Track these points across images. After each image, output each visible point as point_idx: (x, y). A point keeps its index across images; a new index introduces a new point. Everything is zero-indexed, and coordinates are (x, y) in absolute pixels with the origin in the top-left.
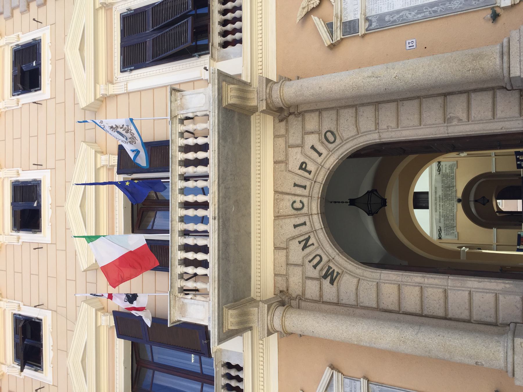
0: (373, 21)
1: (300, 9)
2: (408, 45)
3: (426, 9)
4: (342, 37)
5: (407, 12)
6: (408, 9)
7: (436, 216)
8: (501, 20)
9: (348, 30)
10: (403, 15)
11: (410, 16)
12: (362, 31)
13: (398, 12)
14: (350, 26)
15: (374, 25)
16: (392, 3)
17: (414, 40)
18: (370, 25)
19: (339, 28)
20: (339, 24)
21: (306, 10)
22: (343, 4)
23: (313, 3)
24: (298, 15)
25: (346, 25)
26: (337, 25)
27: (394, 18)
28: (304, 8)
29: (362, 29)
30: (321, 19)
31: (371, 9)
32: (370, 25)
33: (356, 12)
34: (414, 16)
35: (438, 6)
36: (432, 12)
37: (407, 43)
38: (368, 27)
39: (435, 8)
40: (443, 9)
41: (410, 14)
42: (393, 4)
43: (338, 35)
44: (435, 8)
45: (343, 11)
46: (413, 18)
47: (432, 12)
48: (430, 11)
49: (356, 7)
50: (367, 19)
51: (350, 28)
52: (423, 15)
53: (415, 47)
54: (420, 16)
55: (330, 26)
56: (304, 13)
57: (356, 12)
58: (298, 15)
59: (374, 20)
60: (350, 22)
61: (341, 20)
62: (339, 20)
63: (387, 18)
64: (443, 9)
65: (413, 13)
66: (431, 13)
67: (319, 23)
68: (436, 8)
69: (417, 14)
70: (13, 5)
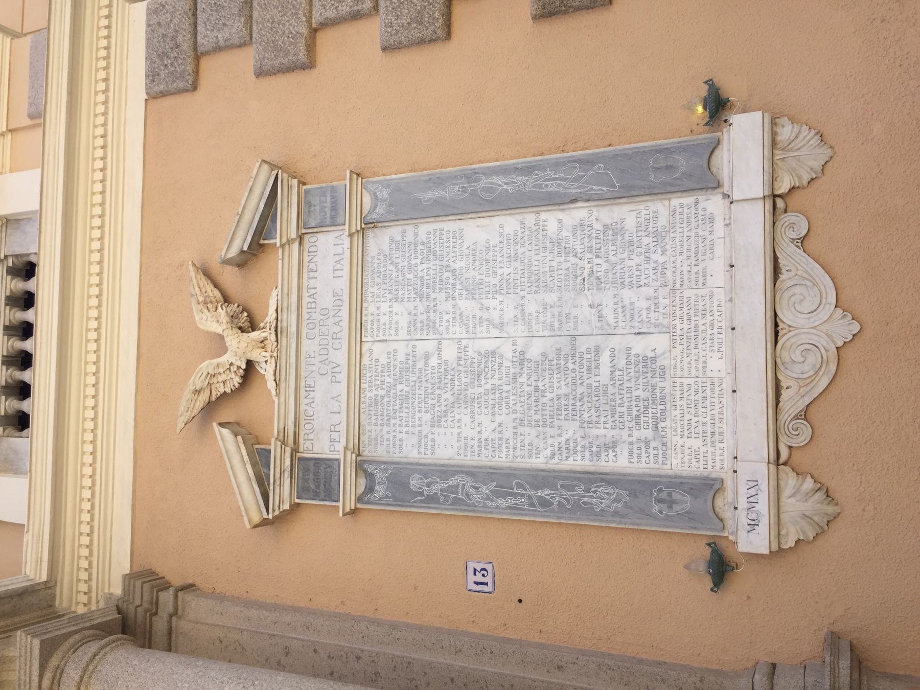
0: (378, 480)
1: (187, 395)
2: (472, 578)
3: (520, 486)
4: (297, 501)
5: (469, 482)
6: (471, 472)
7: (726, 113)
8: (742, 582)
9: (312, 486)
10: (457, 486)
11: (476, 497)
12: (347, 500)
13: (445, 471)
14: (316, 474)
15: (380, 490)
16: (430, 436)
17: (489, 567)
18: (370, 489)
19: (287, 474)
20: (288, 462)
21: (204, 398)
22: (303, 401)
23: (224, 382)
24: (182, 408)
25: (308, 470)
26: (281, 461)
27: (435, 488)
28: (197, 392)
29: (349, 486)
30: (239, 438)
31: (376, 439)
32: (370, 489)
33: (335, 436)
34: (488, 498)
35: (553, 487)
36: (535, 501)
37: (471, 571)
38: (365, 493)
39: (545, 493)
40: (567, 499)
41: (476, 488)
42: (433, 440)
43: (284, 494)
44: (545, 493)
45: (302, 423)
46: (485, 506)
47: (535, 501)
48: (530, 497)
49: (336, 419)
50: (361, 467)
51: (317, 480)
52: (510, 501)
53: (489, 588)
54: (502, 502)
55: (260, 459)
56: (200, 405)
57: (335, 436)
58: (182, 408)
59: (380, 476)
60: (318, 461)
61: (295, 451)
62: (288, 450)
63: (415, 482)
64: (567, 499)
65: (485, 490)
66: (532, 505)
67: (232, 448)
68: (547, 491)
69: (496, 494)
70: (317, 17)
